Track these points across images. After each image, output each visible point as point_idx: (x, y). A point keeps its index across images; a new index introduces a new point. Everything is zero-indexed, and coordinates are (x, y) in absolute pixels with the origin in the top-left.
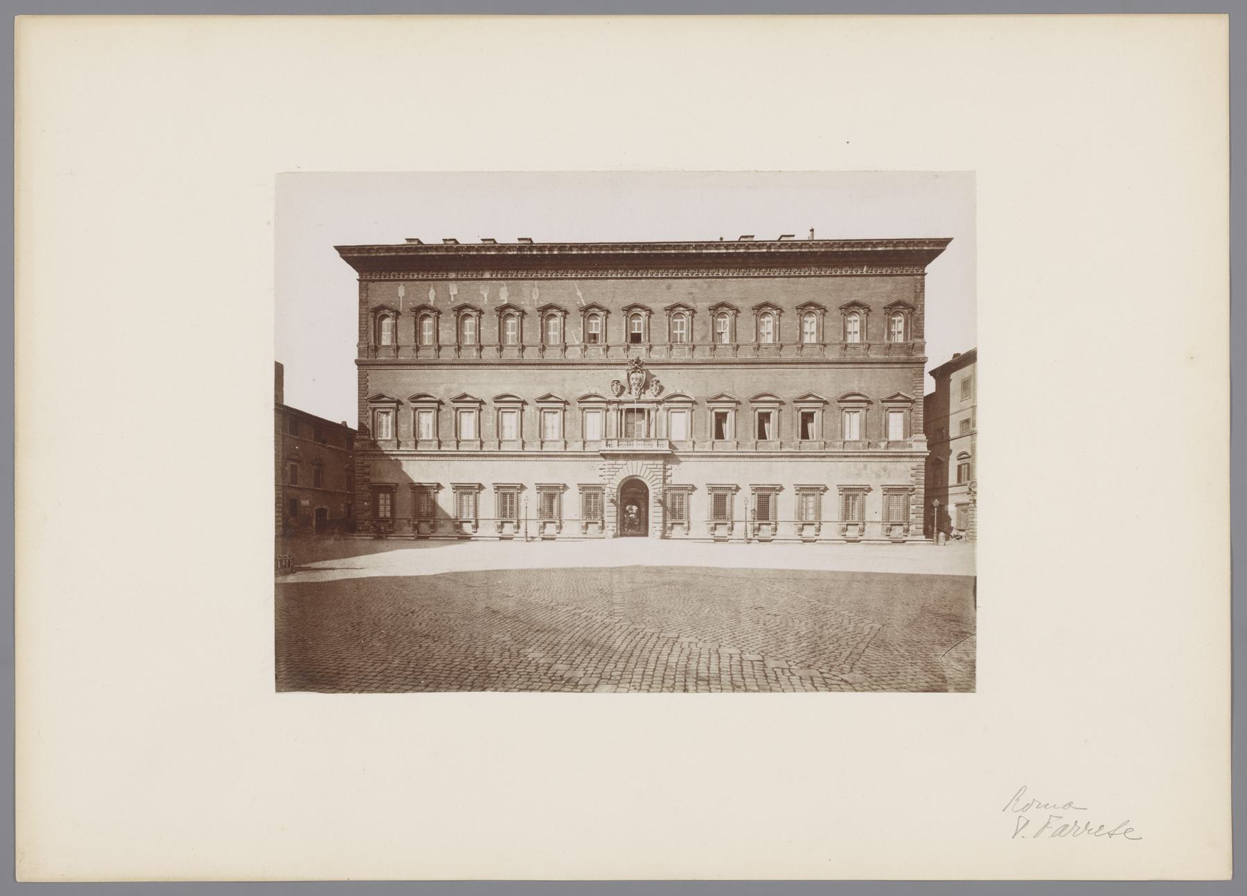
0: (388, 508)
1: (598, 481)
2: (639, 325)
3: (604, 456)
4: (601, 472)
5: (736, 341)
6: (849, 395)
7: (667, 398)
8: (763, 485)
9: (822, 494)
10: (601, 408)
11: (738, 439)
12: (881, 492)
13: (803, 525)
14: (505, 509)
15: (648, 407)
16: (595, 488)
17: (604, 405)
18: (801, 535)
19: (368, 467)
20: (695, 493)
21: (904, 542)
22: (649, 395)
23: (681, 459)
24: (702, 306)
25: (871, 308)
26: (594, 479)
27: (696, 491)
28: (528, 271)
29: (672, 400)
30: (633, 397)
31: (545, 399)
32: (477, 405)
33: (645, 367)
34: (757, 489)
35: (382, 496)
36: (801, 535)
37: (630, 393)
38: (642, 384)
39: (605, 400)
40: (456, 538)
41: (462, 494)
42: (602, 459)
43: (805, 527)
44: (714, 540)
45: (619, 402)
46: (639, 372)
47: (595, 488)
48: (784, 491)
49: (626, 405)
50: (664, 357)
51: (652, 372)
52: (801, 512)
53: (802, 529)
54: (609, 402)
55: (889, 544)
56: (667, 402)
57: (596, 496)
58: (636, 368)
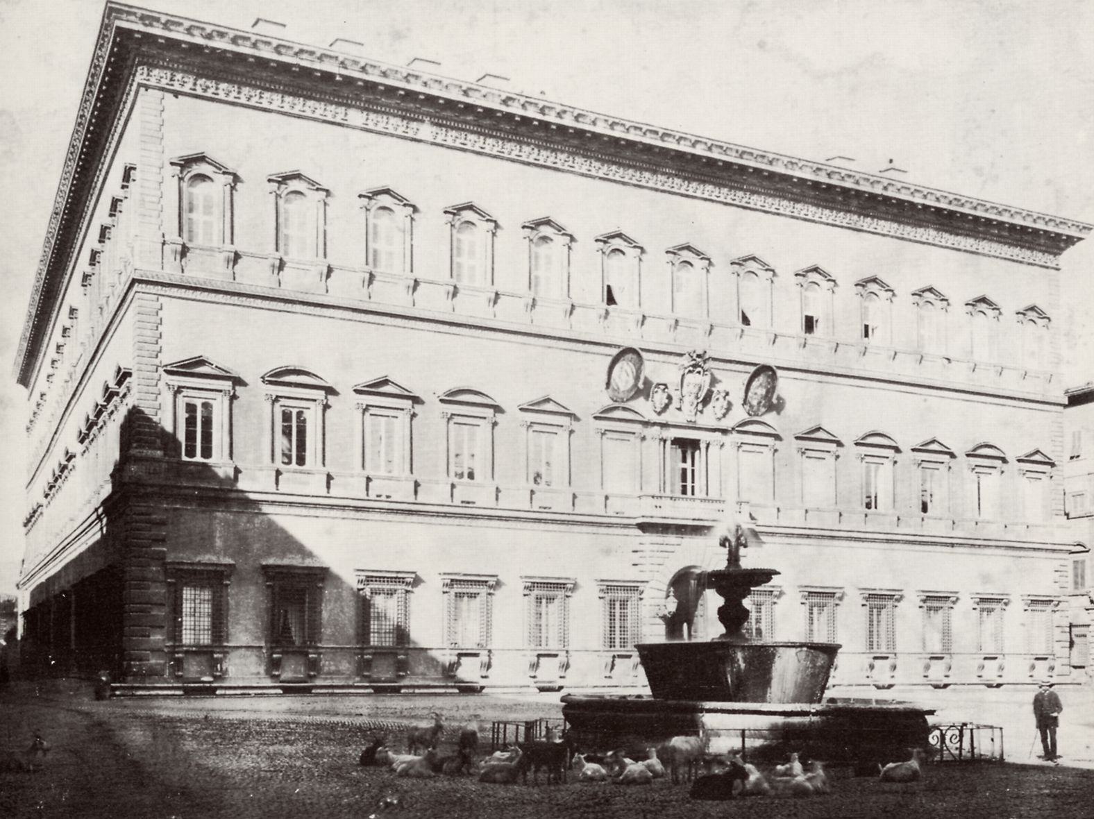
0: (206, 622)
1: (630, 574)
2: (818, 302)
3: (645, 527)
4: (635, 558)
5: (232, 243)
6: (981, 447)
7: (740, 426)
8: (559, 578)
9: (775, 603)
10: (221, 391)
11: (497, 481)
12: (798, 598)
13: (460, 655)
14: (871, 632)
15: (708, 440)
16: (626, 589)
17: (637, 428)
18: (534, 677)
19: (163, 523)
20: (498, 593)
21: (946, 686)
22: (709, 417)
23: (763, 538)
24: (433, 205)
25: (896, 292)
26: (622, 572)
27: (422, 584)
28: (689, 183)
29: (609, 415)
30: (681, 418)
31: (376, 387)
32: (227, 385)
33: (710, 364)
34: (535, 585)
35: (187, 593)
36: (534, 677)
37: (679, 409)
38: (702, 395)
39: (641, 419)
40: (180, 692)
41: (459, 596)
42: (639, 532)
43: (542, 660)
44: (459, 688)
45: (664, 425)
46: (699, 372)
47: (626, 589)
48: (503, 588)
49: (672, 430)
50: (168, 270)
51: (718, 375)
52: (537, 633)
53: (535, 666)
54: (646, 424)
55: (369, 695)
56: (739, 432)
57: (624, 604)
58: (695, 366)
